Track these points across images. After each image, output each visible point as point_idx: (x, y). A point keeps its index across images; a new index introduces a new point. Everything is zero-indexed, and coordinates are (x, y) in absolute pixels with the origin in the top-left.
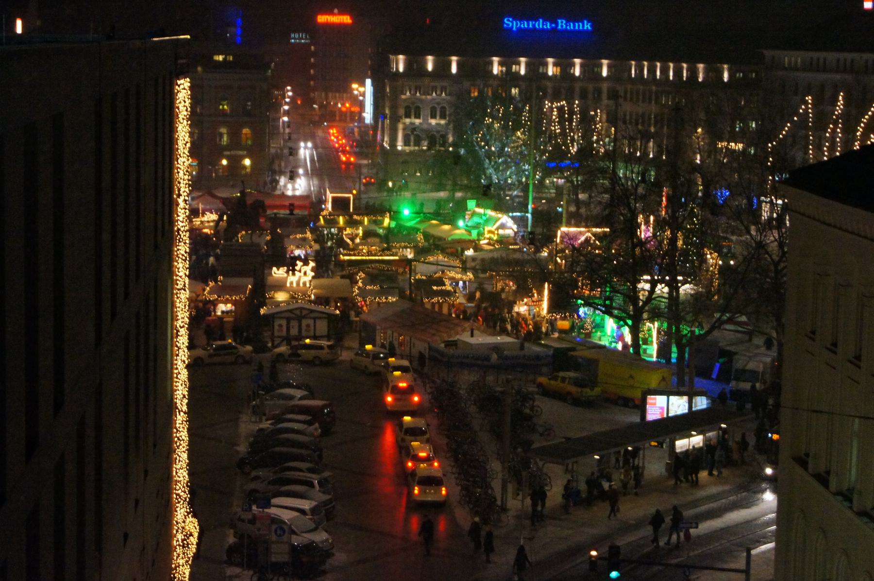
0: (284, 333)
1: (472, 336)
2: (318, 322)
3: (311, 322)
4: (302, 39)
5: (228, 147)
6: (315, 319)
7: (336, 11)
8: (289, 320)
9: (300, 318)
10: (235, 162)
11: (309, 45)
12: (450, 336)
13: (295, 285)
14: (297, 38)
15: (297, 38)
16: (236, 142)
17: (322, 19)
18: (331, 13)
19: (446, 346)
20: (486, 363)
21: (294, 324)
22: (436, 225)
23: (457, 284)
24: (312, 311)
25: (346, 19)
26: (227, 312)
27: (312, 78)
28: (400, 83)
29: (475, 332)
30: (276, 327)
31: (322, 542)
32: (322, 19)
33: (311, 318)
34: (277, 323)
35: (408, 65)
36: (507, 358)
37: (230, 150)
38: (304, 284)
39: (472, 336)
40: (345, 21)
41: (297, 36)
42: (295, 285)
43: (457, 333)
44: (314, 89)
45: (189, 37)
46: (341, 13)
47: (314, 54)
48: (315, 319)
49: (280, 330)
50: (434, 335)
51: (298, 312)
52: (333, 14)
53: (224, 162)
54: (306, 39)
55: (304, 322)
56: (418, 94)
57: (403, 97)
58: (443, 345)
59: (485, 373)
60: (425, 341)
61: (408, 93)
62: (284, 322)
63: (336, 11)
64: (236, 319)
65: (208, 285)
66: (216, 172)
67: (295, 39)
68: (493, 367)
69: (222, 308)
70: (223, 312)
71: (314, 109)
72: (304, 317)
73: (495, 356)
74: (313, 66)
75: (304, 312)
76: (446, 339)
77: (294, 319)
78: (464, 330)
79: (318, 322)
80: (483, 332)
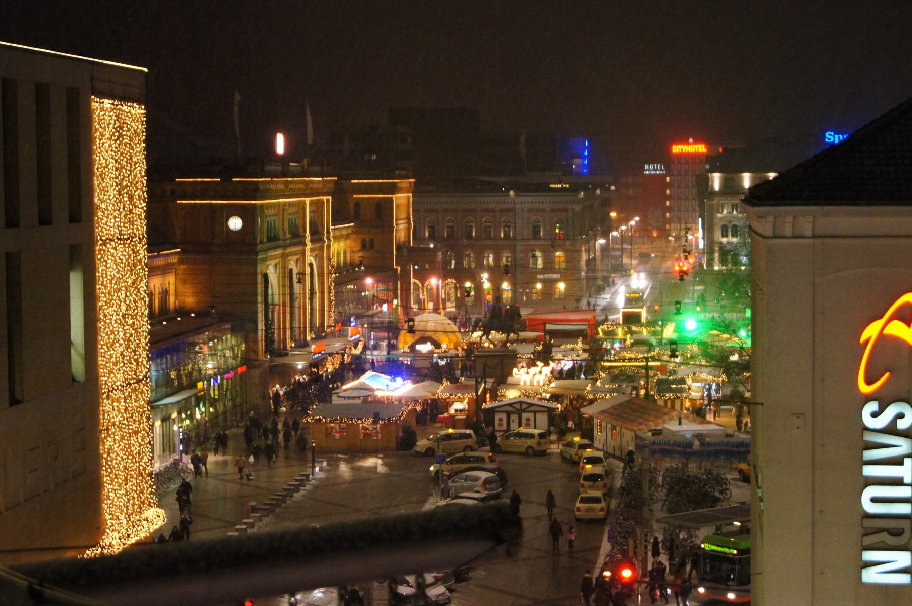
0: (505, 427)
1: (680, 423)
2: (538, 415)
3: (531, 416)
4: (657, 170)
5: (545, 270)
6: (535, 412)
7: (691, 140)
8: (509, 414)
9: (519, 412)
10: (549, 284)
11: (664, 176)
12: (656, 425)
13: (528, 384)
14: (651, 169)
15: (651, 169)
16: (549, 266)
17: (676, 149)
18: (686, 143)
19: (653, 435)
20: (688, 450)
21: (514, 417)
22: (728, 340)
23: (710, 386)
24: (531, 405)
25: (701, 148)
26: (461, 411)
27: (669, 209)
28: (715, 202)
29: (683, 421)
30: (496, 422)
31: (438, 596)
32: (676, 149)
33: (530, 412)
34: (497, 417)
35: (725, 183)
36: (709, 444)
37: (544, 273)
38: (538, 382)
39: (680, 423)
40: (700, 150)
41: (651, 167)
42: (528, 384)
43: (664, 422)
44: (670, 221)
45: (146, 70)
46: (696, 142)
47: (669, 186)
48: (535, 412)
49: (500, 425)
50: (642, 424)
51: (518, 406)
52: (688, 144)
53: (539, 286)
54: (661, 170)
55: (525, 416)
56: (735, 212)
57: (719, 215)
58: (649, 434)
59: (687, 459)
60: (632, 430)
61: (725, 212)
62: (504, 416)
63: (691, 140)
64: (468, 416)
65: (442, 384)
66: (528, 295)
67: (649, 170)
68: (695, 454)
69: (458, 406)
70: (456, 411)
71: (670, 241)
72: (525, 411)
73: (697, 443)
74: (669, 198)
75: (524, 406)
76: (653, 428)
77: (513, 413)
78: (671, 419)
79: (538, 415)
80: (694, 421)
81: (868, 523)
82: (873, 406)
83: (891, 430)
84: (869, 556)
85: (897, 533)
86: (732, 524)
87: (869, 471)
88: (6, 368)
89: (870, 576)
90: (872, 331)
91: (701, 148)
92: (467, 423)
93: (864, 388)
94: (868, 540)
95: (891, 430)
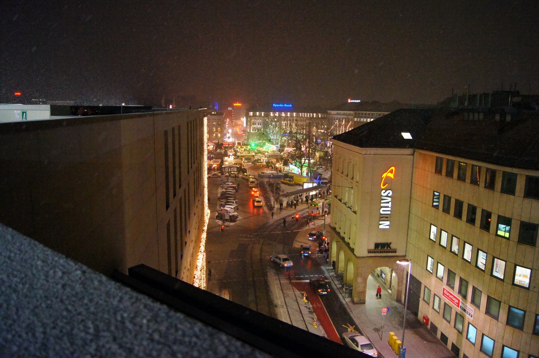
9: (231, 168)
10: (217, 135)
15: (230, 109)
16: (217, 131)
32: (235, 105)
35: (253, 114)
81: (381, 216)
82: (384, 191)
83: (387, 196)
84: (381, 222)
85: (387, 218)
86: (54, 111)
87: (382, 205)
88: (165, 175)
89: (381, 227)
90: (384, 175)
91: (240, 105)
92: (218, 170)
93: (382, 187)
94: (381, 219)
95: (387, 196)
